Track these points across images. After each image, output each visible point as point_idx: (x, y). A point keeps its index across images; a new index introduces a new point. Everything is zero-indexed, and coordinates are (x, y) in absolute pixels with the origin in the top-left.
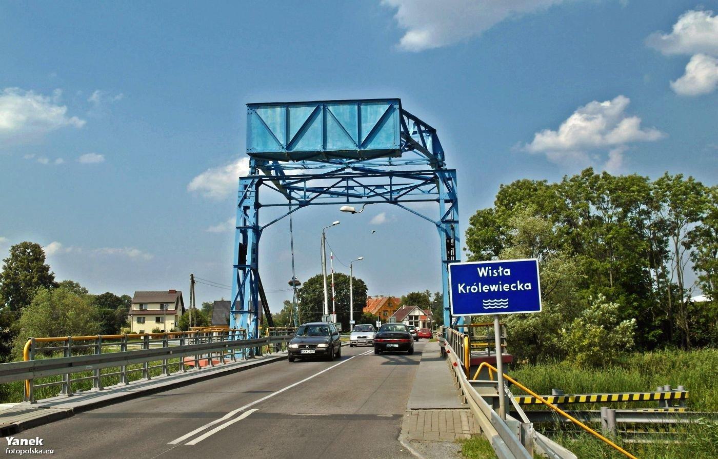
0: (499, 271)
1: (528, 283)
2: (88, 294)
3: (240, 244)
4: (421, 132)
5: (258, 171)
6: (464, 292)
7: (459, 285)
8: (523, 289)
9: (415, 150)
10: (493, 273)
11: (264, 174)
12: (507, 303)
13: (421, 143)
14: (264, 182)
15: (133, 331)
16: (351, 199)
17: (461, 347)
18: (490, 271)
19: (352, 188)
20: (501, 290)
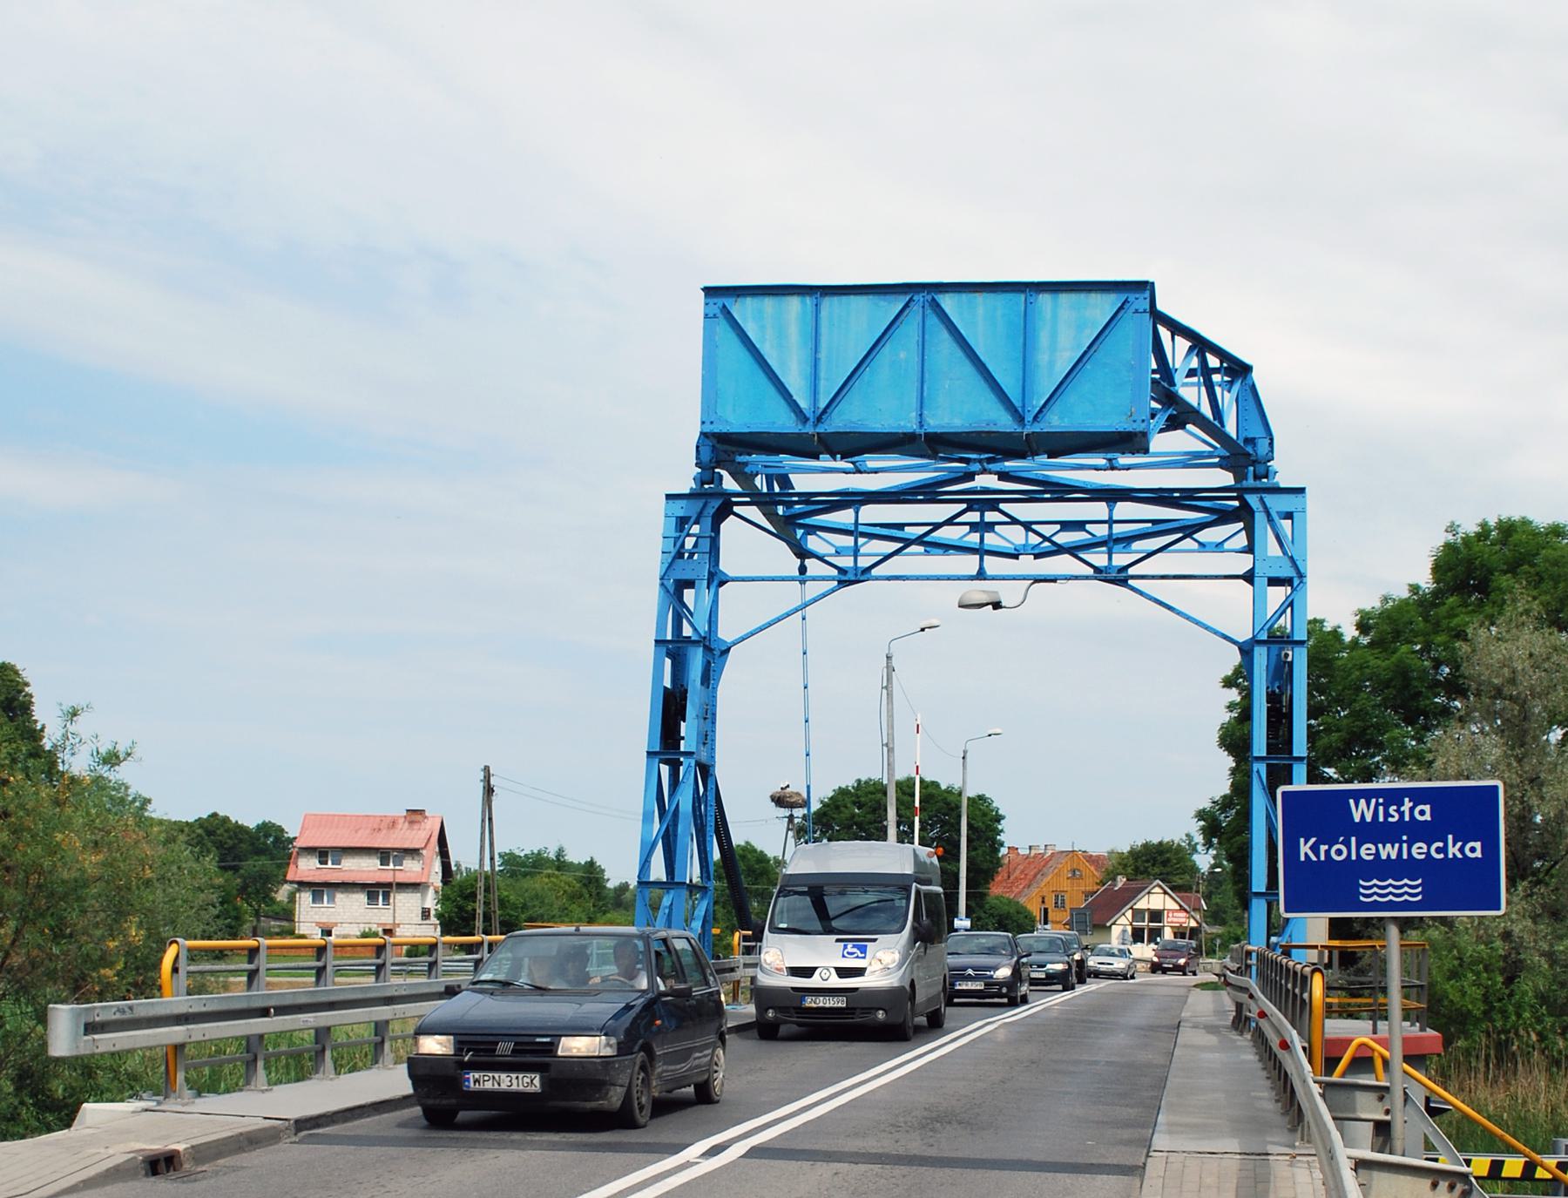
0: (1402, 809)
1: (1476, 841)
3: (665, 688)
4: (1206, 372)
5: (721, 477)
6: (1314, 858)
7: (1302, 840)
8: (1459, 856)
9: (1189, 427)
10: (1387, 815)
12: (1420, 889)
13: (1206, 410)
14: (736, 509)
15: (301, 932)
16: (993, 565)
17: (1303, 1001)
18: (1381, 808)
19: (990, 527)
20: (1405, 856)
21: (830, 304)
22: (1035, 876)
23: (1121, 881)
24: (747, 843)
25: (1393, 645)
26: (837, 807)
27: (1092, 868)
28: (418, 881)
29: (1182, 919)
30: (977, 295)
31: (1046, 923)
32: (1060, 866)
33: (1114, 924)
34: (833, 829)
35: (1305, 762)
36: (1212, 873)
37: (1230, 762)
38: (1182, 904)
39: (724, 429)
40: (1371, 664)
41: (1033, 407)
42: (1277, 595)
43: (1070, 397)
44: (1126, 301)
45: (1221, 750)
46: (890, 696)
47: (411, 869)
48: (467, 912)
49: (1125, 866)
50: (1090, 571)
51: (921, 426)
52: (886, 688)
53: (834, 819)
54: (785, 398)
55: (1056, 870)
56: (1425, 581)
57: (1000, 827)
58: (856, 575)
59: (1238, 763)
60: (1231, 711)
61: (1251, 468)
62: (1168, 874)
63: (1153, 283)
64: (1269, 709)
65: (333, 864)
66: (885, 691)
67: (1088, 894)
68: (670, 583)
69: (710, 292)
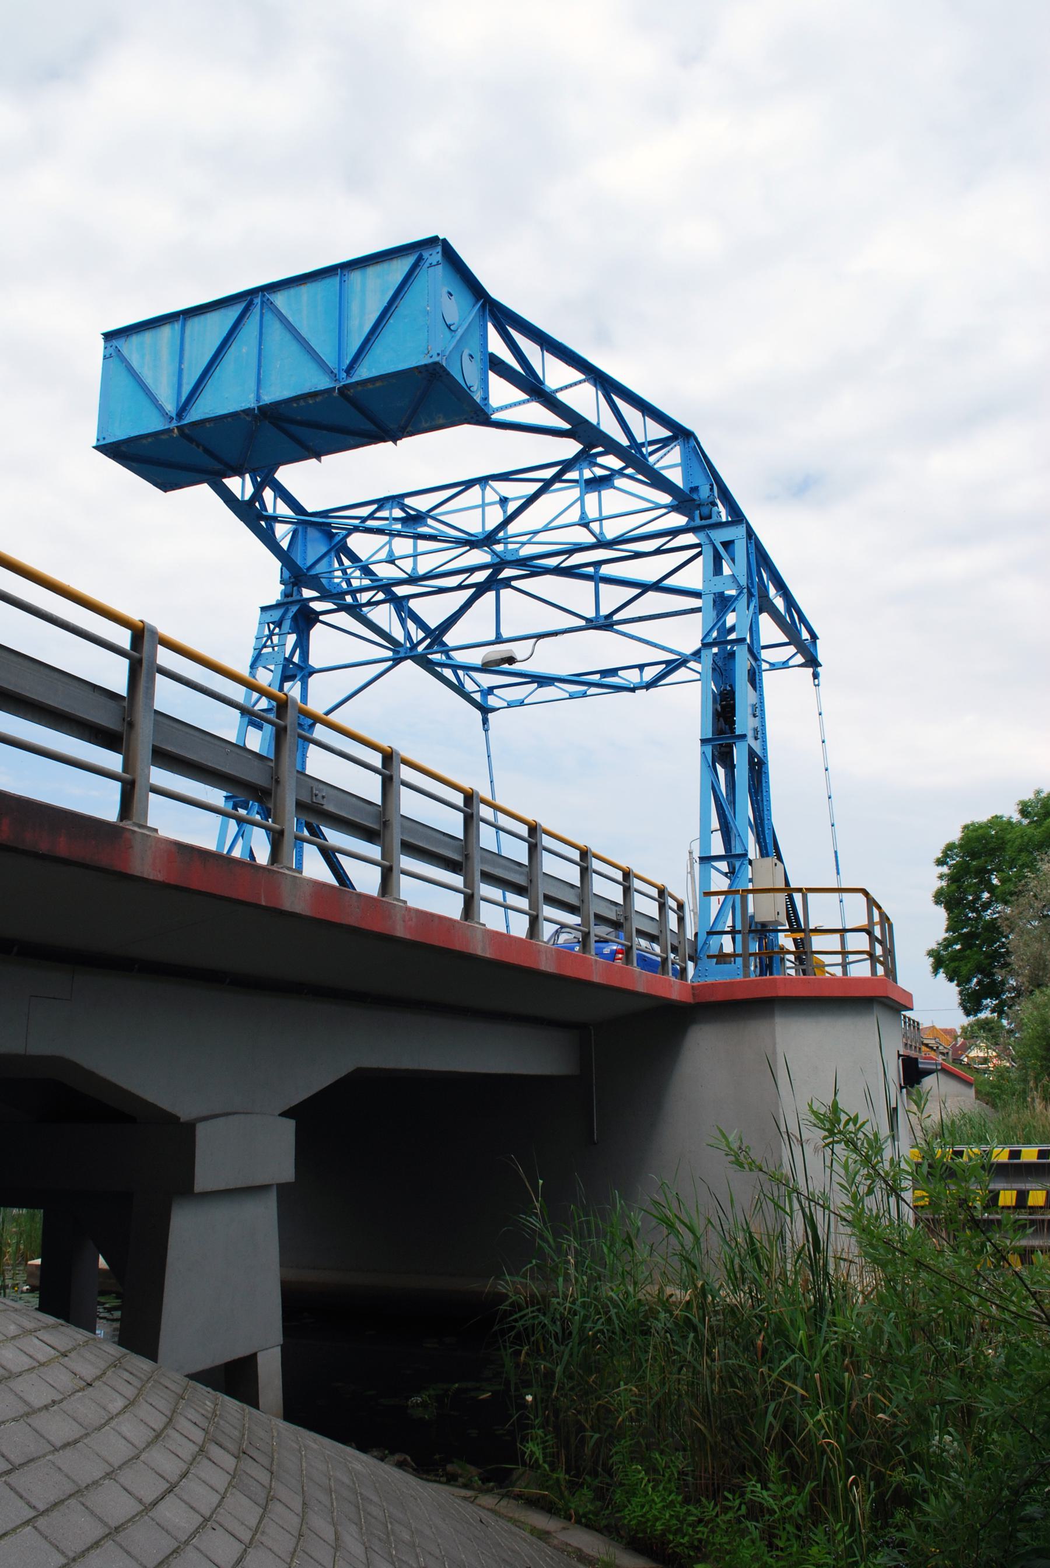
14: (321, 618)
50: (583, 623)
51: (258, 401)
66: (689, 875)
69: (109, 336)
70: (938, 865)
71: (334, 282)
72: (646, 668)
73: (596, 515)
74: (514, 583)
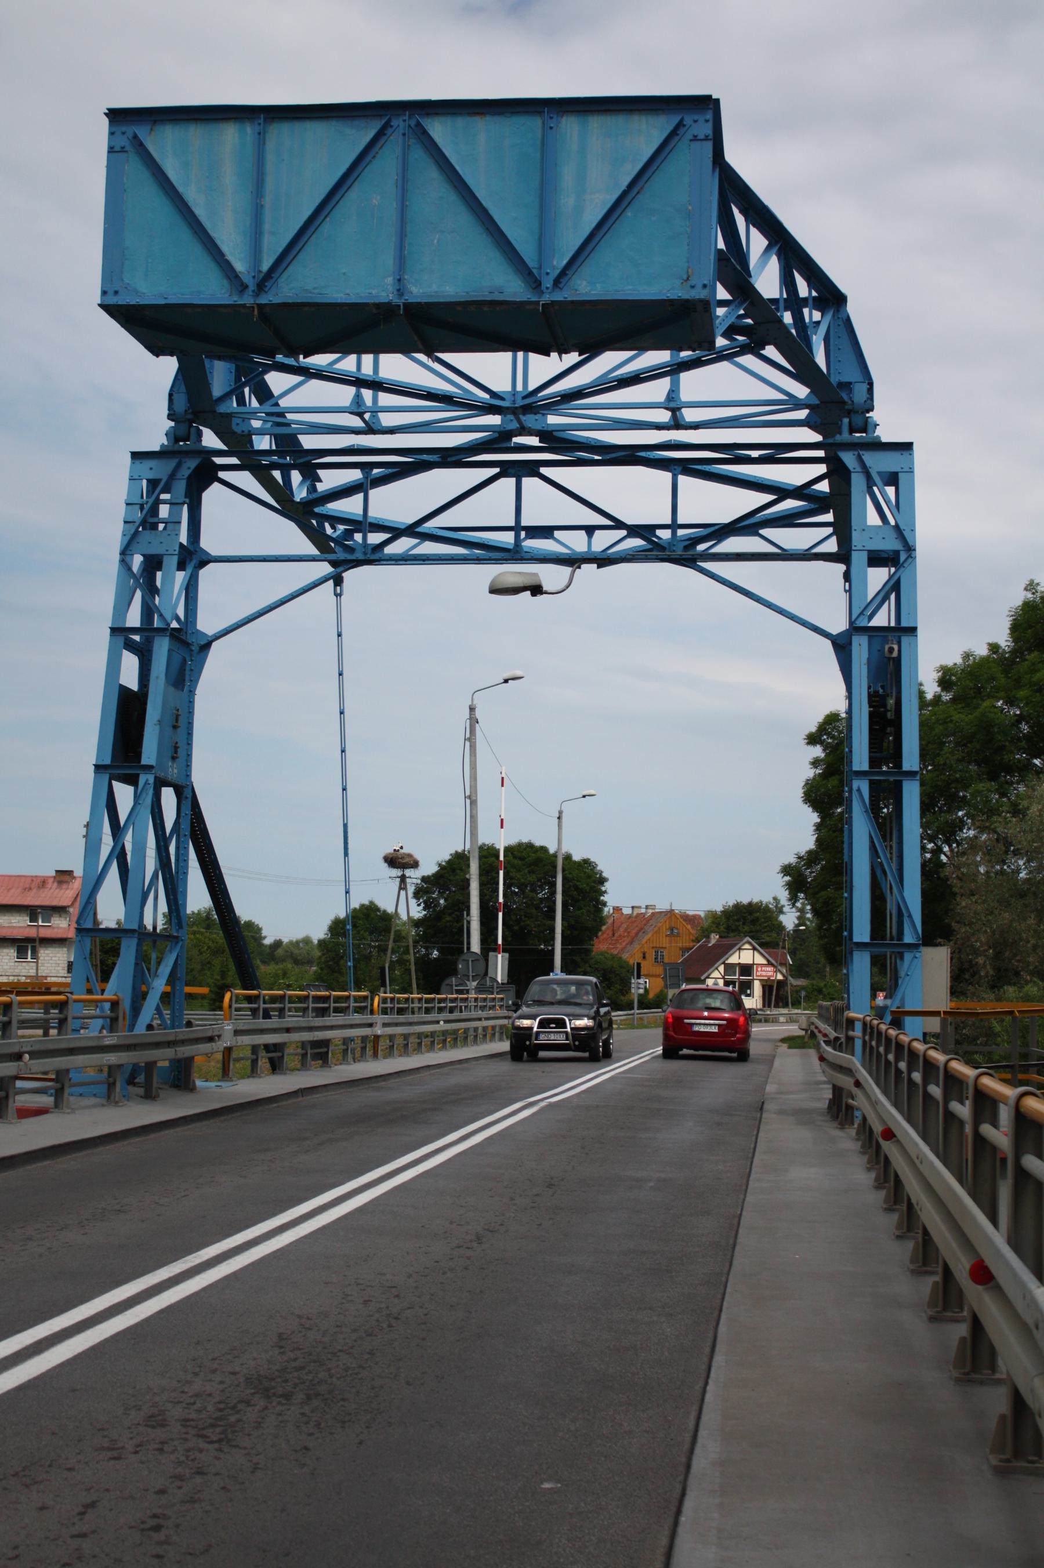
2: (123, 921)
11: (219, 445)
14: (222, 475)
21: (281, 133)
22: (637, 934)
23: (714, 938)
24: (371, 903)
25: (975, 701)
26: (453, 870)
27: (689, 927)
28: (65, 936)
29: (768, 972)
30: (477, 119)
31: (639, 977)
32: (659, 925)
33: (708, 977)
34: (449, 889)
35: (918, 777)
36: (796, 931)
37: (815, 818)
38: (770, 959)
39: (133, 300)
40: (954, 718)
41: (554, 268)
42: (877, 577)
43: (604, 254)
44: (680, 125)
45: (807, 806)
46: (473, 748)
47: (61, 925)
48: (107, 966)
49: (718, 925)
51: (400, 292)
52: (469, 739)
53: (450, 880)
54: (215, 260)
55: (656, 929)
56: (1003, 638)
57: (603, 889)
58: (365, 553)
59: (823, 818)
60: (816, 768)
61: (846, 421)
62: (757, 931)
63: (717, 101)
64: (872, 715)
65: (42, 922)
66: (468, 744)
67: (684, 950)
68: (137, 561)
69: (117, 116)
70: (808, 743)
71: (534, 124)
72: (597, 532)
73: (685, 396)
74: (544, 471)
